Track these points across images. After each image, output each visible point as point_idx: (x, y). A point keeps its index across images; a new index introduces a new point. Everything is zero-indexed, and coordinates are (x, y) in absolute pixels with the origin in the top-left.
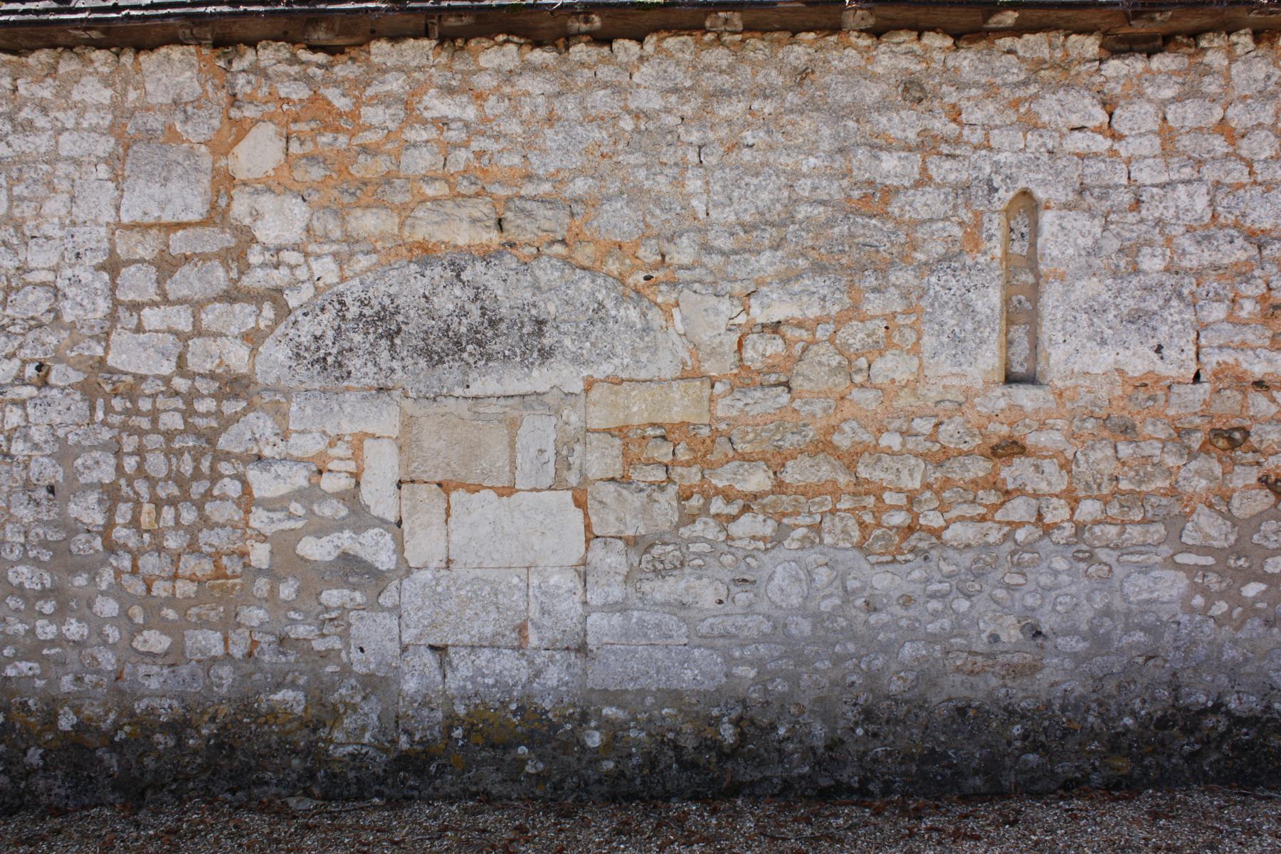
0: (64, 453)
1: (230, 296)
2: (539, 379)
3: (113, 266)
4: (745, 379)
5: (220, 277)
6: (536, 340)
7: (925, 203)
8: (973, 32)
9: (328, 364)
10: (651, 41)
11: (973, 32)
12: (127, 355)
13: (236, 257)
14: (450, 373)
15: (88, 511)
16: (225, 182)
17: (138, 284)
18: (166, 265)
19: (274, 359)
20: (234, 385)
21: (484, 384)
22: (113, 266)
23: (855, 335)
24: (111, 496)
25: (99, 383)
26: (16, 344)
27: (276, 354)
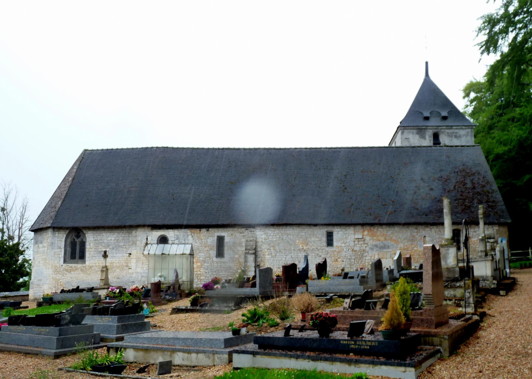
0: (351, 256)
1: (364, 244)
2: (389, 250)
3: (354, 241)
4: (404, 249)
5: (363, 242)
6: (388, 247)
7: (417, 236)
8: (158, 303)
9: (372, 249)
10: (33, 359)
11: (158, 303)
12: (355, 249)
13: (364, 241)
14: (382, 250)
15: (353, 261)
16: (363, 235)
17: (356, 243)
18: (358, 241)
19: (367, 249)
20: (364, 251)
21: (384, 250)
22: (354, 241)
23: (413, 246)
24: (355, 259)
25: (353, 250)
26: (168, 292)
27: (367, 249)
